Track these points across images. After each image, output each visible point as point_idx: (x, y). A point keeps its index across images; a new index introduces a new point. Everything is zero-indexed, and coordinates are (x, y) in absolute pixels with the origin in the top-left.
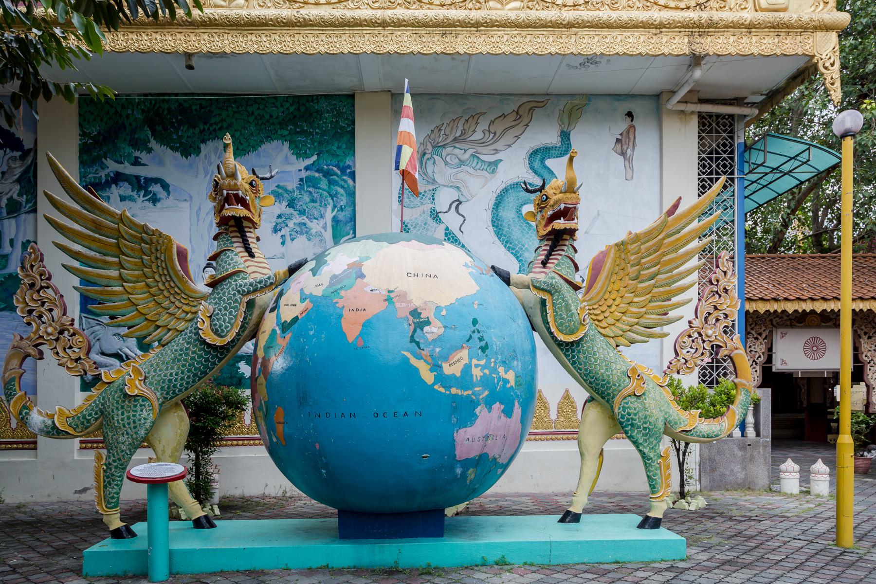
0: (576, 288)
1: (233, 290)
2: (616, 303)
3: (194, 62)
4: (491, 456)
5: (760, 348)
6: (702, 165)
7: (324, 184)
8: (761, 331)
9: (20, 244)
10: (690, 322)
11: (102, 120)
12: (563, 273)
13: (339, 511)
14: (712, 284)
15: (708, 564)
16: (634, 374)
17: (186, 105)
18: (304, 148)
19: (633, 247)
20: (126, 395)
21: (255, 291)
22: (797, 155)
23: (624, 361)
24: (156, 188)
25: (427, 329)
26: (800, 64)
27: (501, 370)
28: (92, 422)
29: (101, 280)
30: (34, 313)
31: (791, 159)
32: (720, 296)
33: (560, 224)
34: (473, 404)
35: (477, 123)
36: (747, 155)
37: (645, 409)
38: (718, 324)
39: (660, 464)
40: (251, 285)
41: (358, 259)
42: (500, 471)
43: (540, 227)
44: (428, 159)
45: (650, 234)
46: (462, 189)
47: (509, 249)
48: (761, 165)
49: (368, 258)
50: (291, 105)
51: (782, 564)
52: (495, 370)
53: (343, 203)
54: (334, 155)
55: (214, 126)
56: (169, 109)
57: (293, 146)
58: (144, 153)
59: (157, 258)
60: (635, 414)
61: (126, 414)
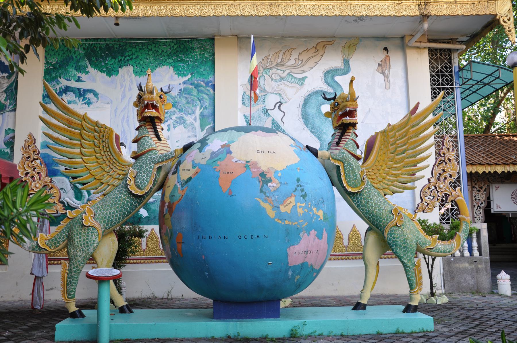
0: (358, 159)
1: (149, 161)
2: (383, 168)
3: (119, 22)
4: (309, 264)
5: (482, 197)
6: (433, 79)
7: (195, 92)
8: (482, 185)
9: (4, 130)
10: (429, 180)
11: (59, 55)
12: (350, 150)
13: (214, 301)
14: (441, 156)
15: (449, 334)
16: (396, 212)
17: (111, 45)
18: (183, 70)
19: (391, 133)
20: (83, 226)
21: (162, 161)
22: (492, 74)
23: (389, 204)
24: (90, 96)
25: (270, 184)
26: (490, 19)
27: (315, 209)
28: (61, 243)
29: (69, 154)
30: (29, 175)
31: (489, 75)
32: (446, 163)
33: (347, 119)
34: (298, 230)
35: (291, 55)
36: (460, 73)
37: (404, 235)
38: (446, 181)
39: (415, 270)
40: (160, 157)
41: (227, 142)
42: (315, 274)
43: (334, 121)
44: (260, 76)
45: (403, 125)
46: (283, 95)
47: (313, 133)
48: (471, 79)
49: (233, 142)
50: (175, 44)
51: (496, 334)
52: (311, 210)
53: (207, 104)
54: (201, 74)
55: (128, 58)
56: (100, 47)
57: (176, 69)
58: (84, 74)
59: (103, 141)
60: (398, 238)
61: (82, 238)
